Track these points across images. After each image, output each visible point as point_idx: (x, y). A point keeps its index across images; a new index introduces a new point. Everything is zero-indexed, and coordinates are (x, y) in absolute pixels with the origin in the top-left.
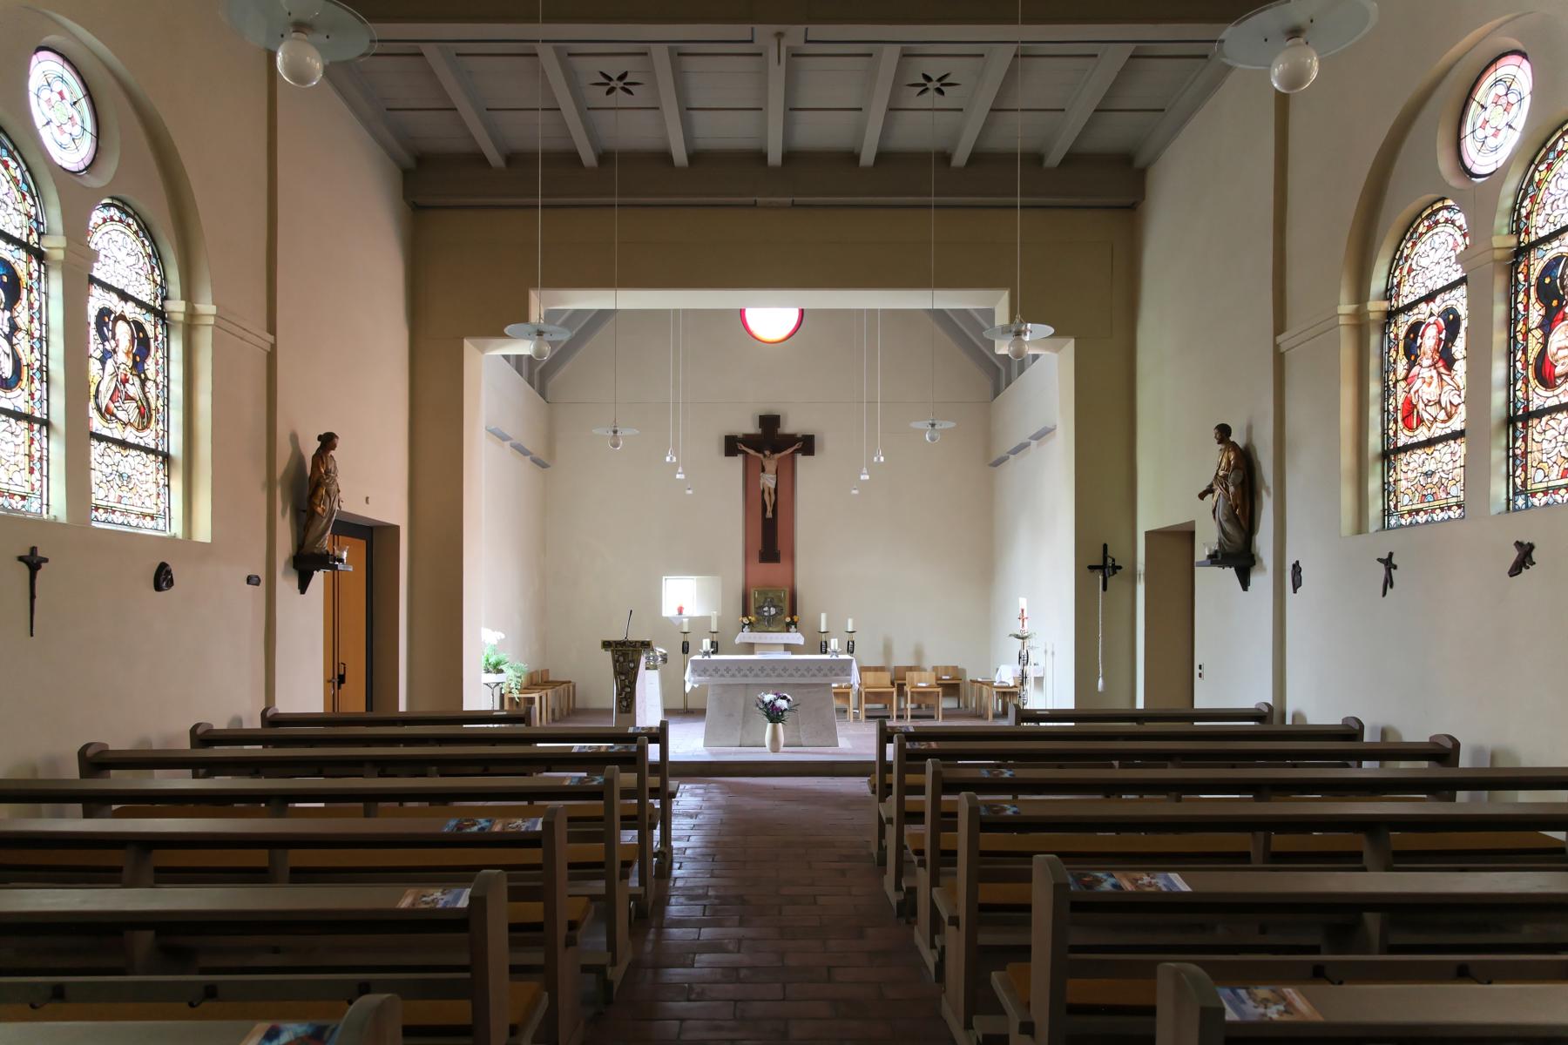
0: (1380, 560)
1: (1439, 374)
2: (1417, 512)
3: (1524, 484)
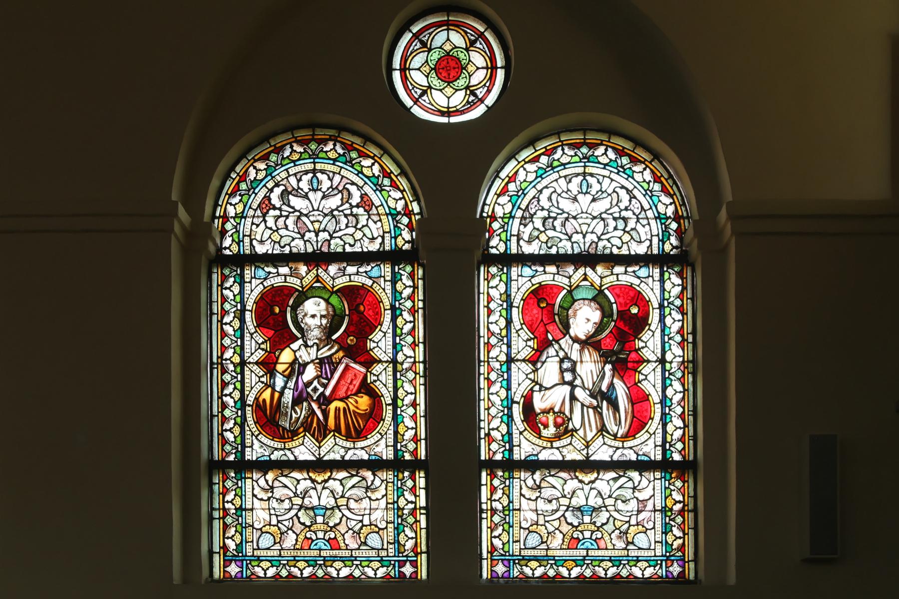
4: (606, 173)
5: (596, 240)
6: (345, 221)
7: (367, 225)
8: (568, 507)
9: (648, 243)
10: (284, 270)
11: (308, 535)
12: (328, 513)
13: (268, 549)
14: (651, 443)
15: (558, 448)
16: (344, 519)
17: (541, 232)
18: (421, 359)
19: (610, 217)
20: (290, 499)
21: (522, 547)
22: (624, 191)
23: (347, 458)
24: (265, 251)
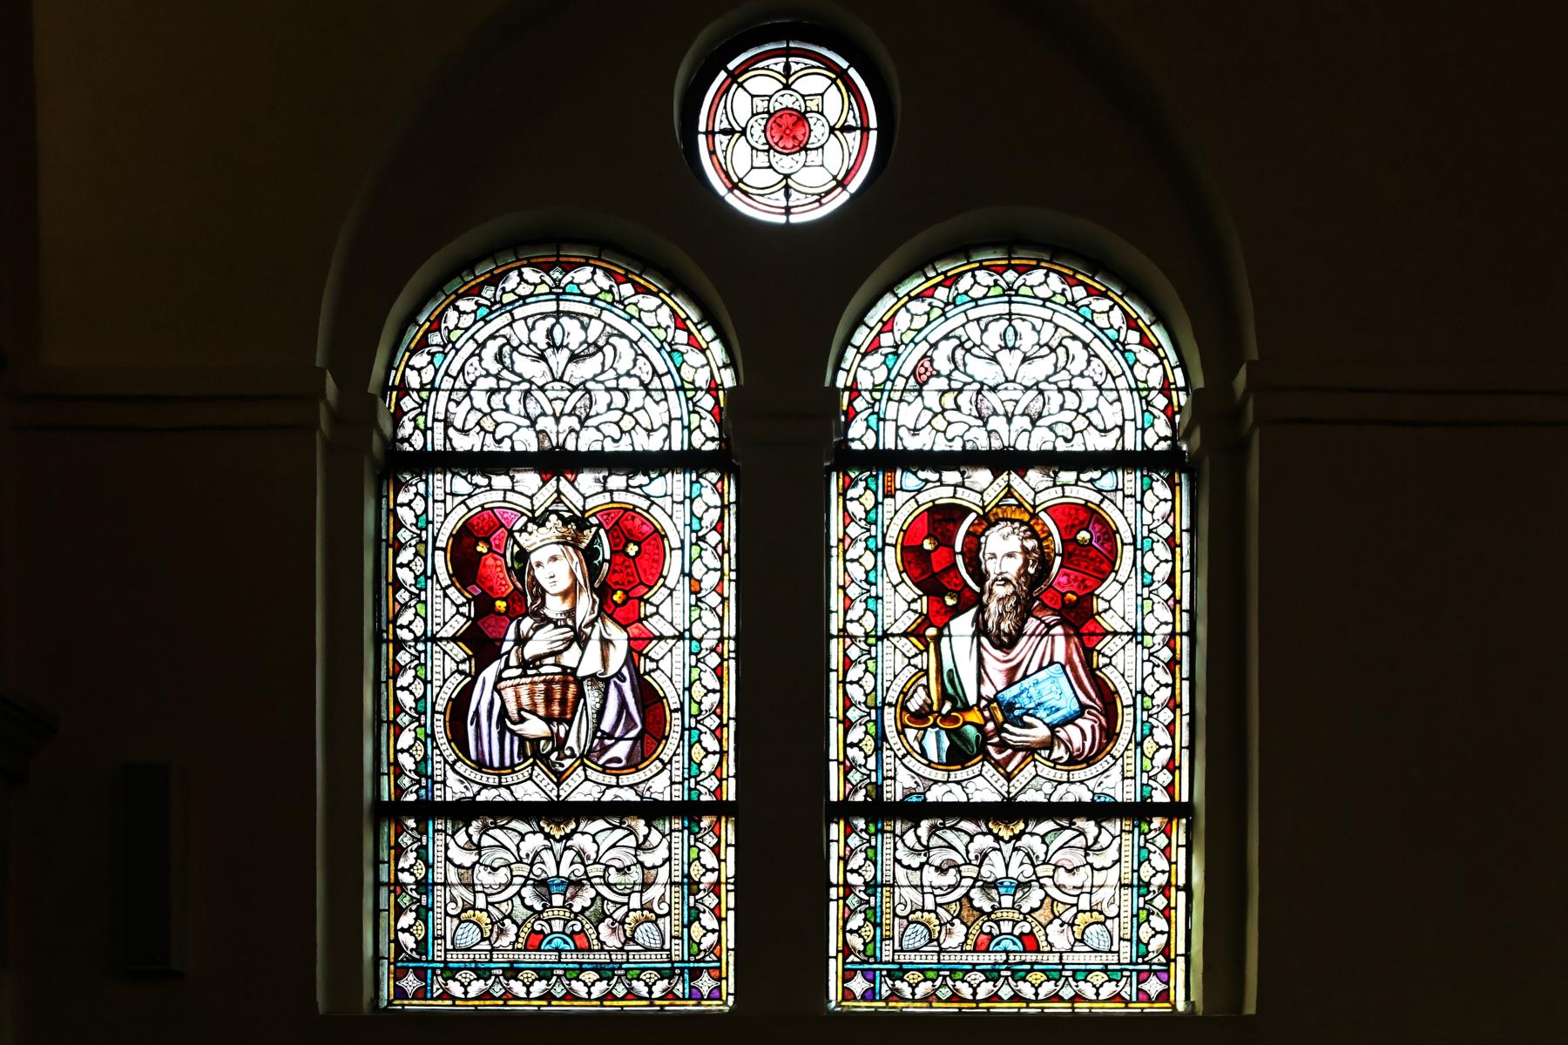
4: (1047, 314)
5: (577, 427)
6: (1059, 398)
7: (1096, 408)
8: (976, 880)
9: (664, 431)
11: (537, 928)
12: (571, 890)
13: (917, 950)
14: (1116, 772)
15: (958, 783)
16: (1048, 900)
17: (485, 415)
18: (733, 633)
19: (601, 386)
20: (509, 865)
21: (449, 946)
22: (626, 342)
23: (1054, 799)
24: (468, 448)
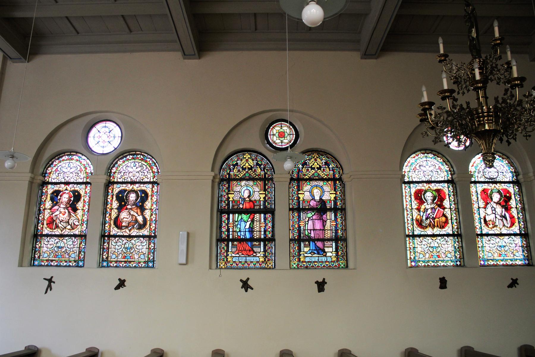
0: (241, 280)
1: (69, 212)
2: (52, 261)
3: (107, 258)
10: (59, 186)
